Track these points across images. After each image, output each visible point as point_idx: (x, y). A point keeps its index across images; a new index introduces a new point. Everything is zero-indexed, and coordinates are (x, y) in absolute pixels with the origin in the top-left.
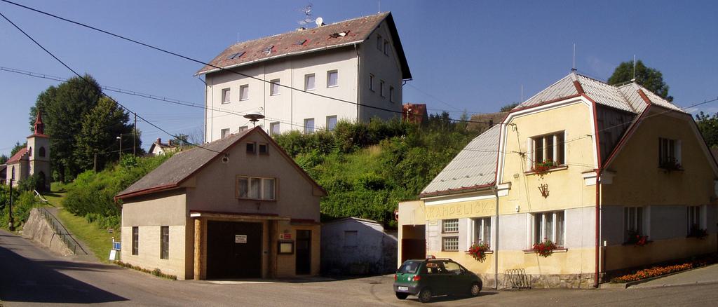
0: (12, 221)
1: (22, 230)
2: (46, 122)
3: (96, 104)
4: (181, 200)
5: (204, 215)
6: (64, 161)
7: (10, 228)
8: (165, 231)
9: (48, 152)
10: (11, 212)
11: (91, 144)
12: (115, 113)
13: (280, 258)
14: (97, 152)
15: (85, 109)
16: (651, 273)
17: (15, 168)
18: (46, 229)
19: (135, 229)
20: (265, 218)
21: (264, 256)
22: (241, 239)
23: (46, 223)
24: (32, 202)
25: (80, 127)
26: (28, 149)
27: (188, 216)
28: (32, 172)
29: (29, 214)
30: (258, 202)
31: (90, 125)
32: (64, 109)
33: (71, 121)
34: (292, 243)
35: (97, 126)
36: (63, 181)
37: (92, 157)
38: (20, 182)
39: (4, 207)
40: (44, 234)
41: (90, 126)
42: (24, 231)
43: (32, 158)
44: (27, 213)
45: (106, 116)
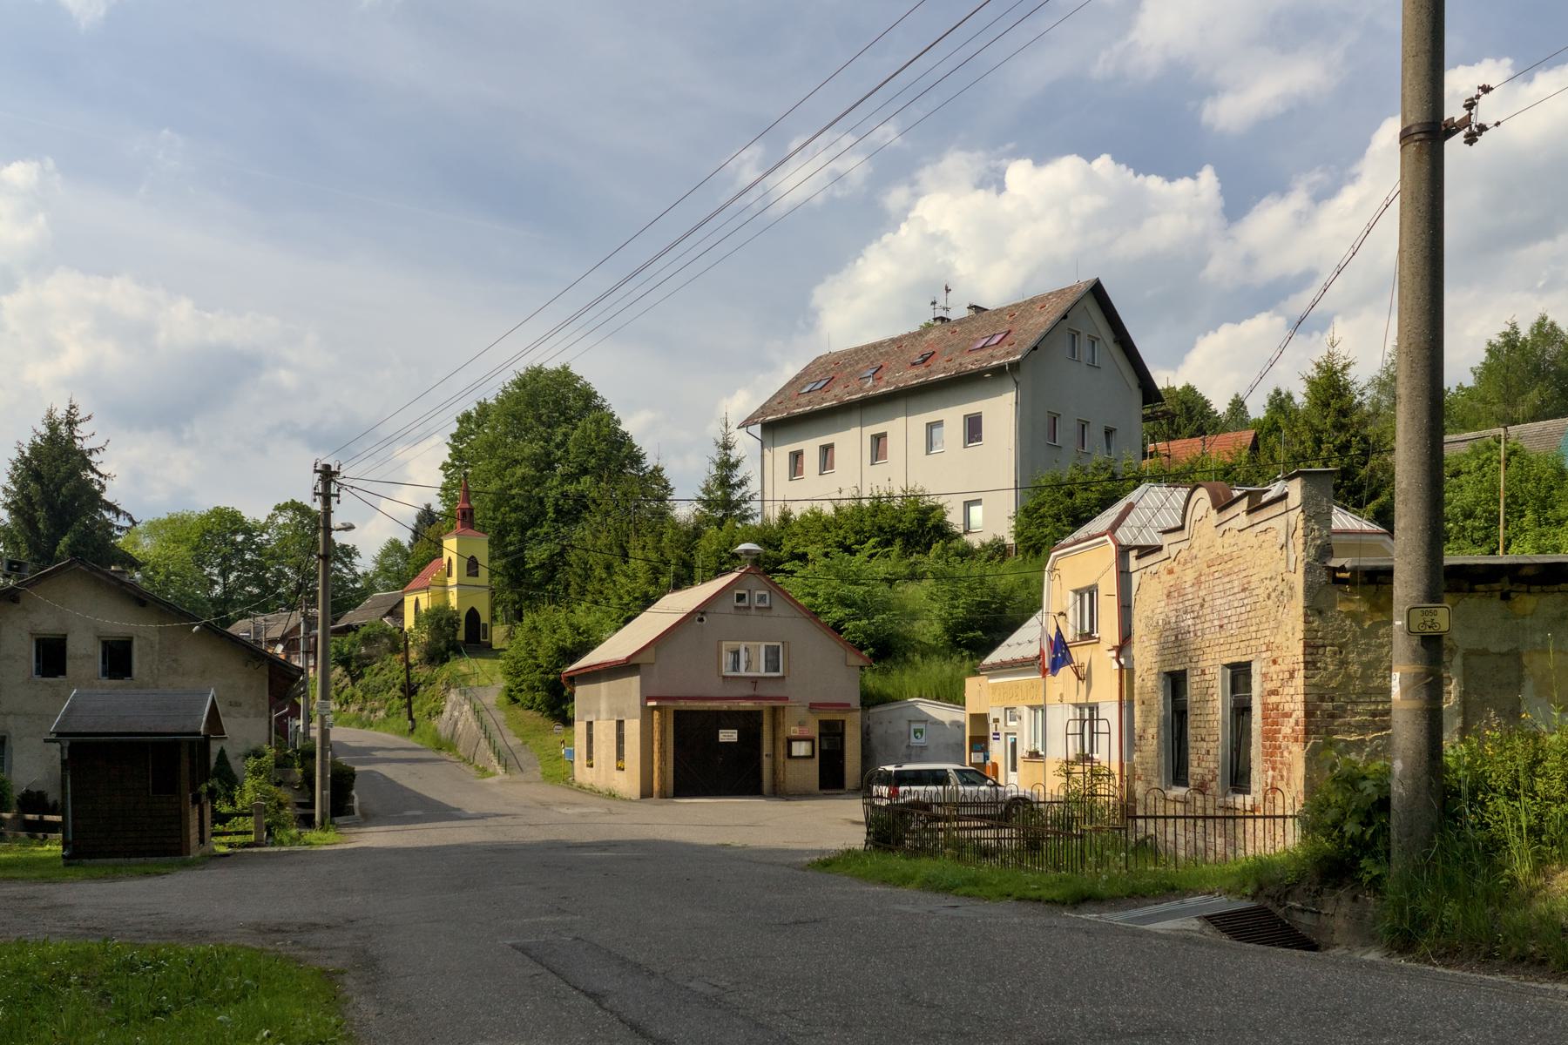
4: (634, 682)
5: (663, 703)
8: (620, 724)
13: (791, 764)
16: (318, 718)
19: (590, 724)
20: (766, 704)
21: (766, 764)
22: (728, 736)
26: (445, 561)
27: (644, 707)
30: (755, 681)
34: (812, 741)
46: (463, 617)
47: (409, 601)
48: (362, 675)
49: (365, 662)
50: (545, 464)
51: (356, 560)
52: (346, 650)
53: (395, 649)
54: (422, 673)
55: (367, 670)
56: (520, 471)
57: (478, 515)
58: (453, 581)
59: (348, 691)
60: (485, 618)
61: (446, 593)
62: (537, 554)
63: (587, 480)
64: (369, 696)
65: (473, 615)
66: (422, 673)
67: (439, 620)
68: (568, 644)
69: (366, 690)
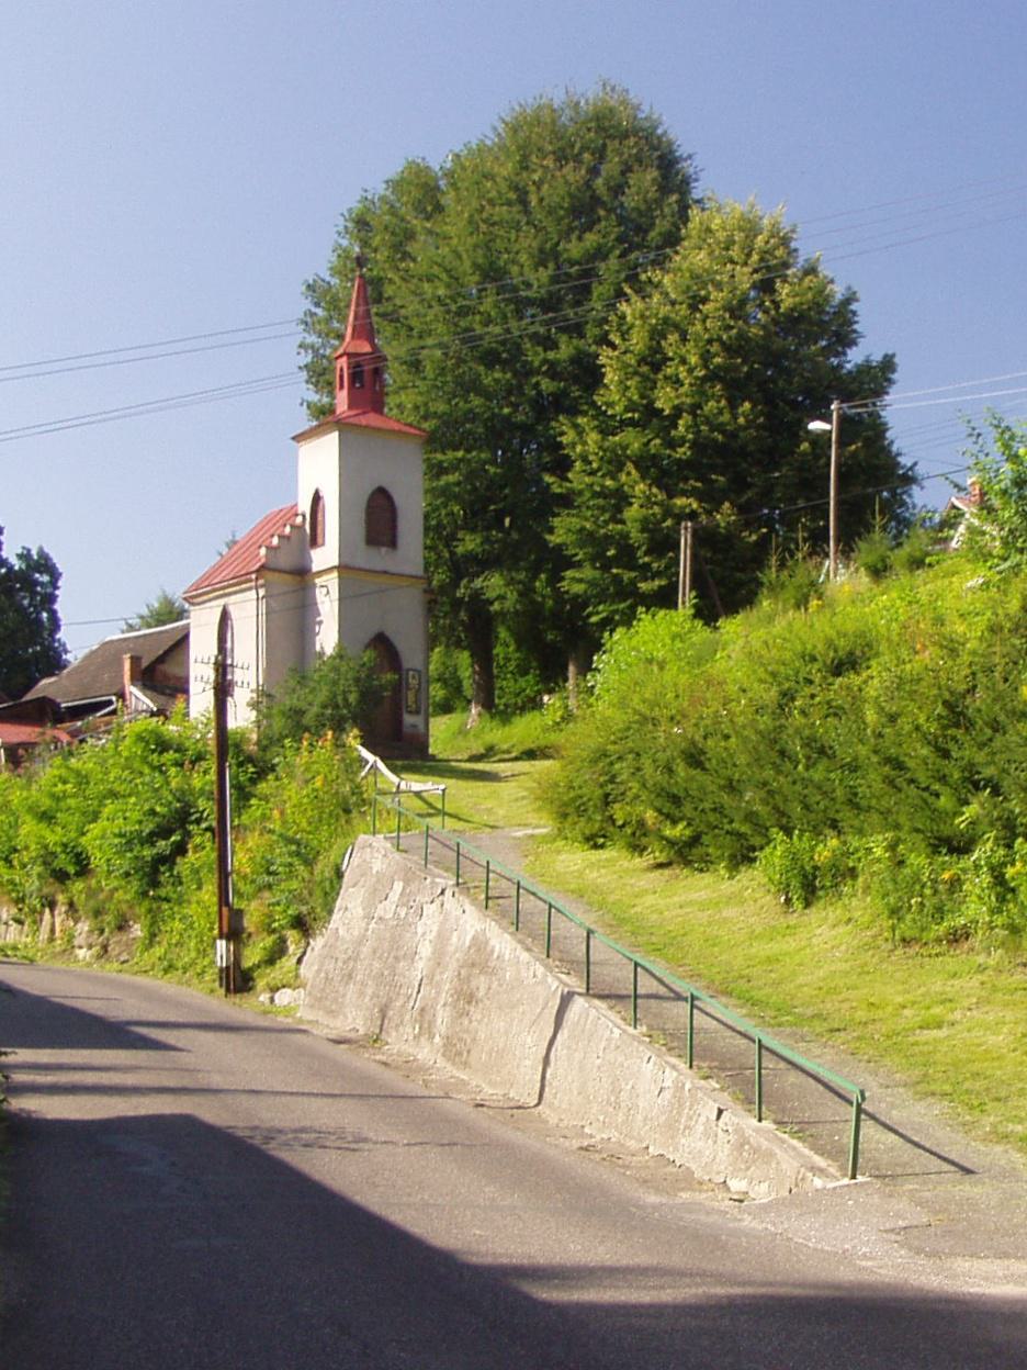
0: (234, 932)
1: (294, 983)
2: (394, 349)
3: (673, 239)
6: (493, 584)
7: (225, 974)
9: (412, 506)
10: (223, 874)
11: (662, 474)
12: (784, 291)
14: (693, 516)
15: (610, 268)
17: (234, 612)
18: (479, 959)
23: (469, 921)
24: (348, 808)
25: (588, 374)
28: (327, 638)
29: (339, 875)
31: (642, 360)
32: (492, 273)
33: (537, 339)
35: (686, 361)
36: (488, 705)
37: (663, 544)
38: (264, 700)
39: (180, 849)
40: (466, 998)
41: (654, 338)
42: (312, 992)
43: (325, 556)
44: (323, 868)
45: (736, 310)
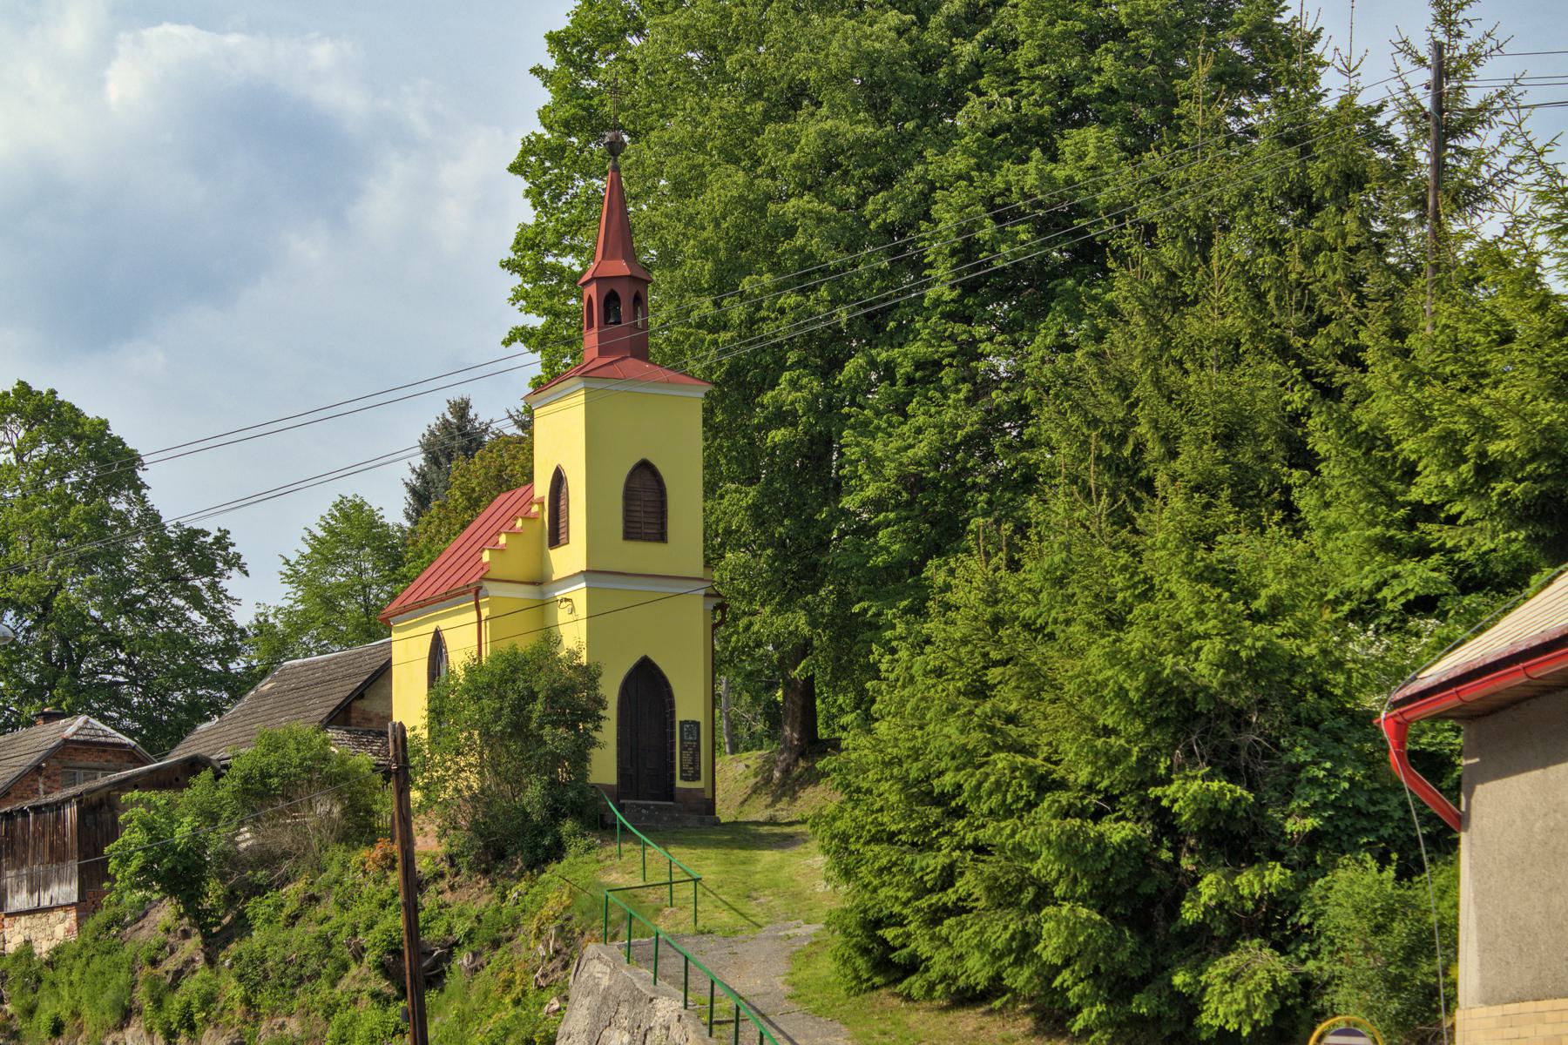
46: (610, 689)
47: (408, 650)
48: (242, 926)
49: (252, 879)
50: (915, 95)
51: (232, 583)
52: (181, 834)
53: (358, 828)
54: (461, 905)
55: (258, 908)
56: (810, 130)
57: (660, 308)
58: (569, 558)
59: (192, 985)
60: (689, 704)
61: (543, 606)
62: (887, 451)
63: (1088, 140)
64: (264, 999)
65: (647, 685)
66: (461, 905)
67: (521, 702)
68: (1204, 669)
69: (254, 977)
